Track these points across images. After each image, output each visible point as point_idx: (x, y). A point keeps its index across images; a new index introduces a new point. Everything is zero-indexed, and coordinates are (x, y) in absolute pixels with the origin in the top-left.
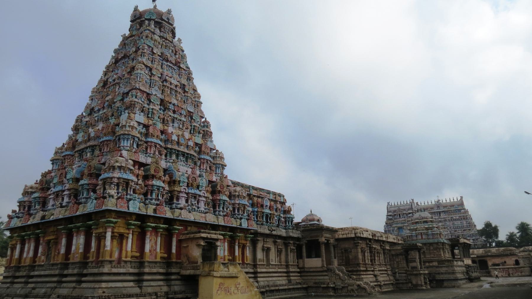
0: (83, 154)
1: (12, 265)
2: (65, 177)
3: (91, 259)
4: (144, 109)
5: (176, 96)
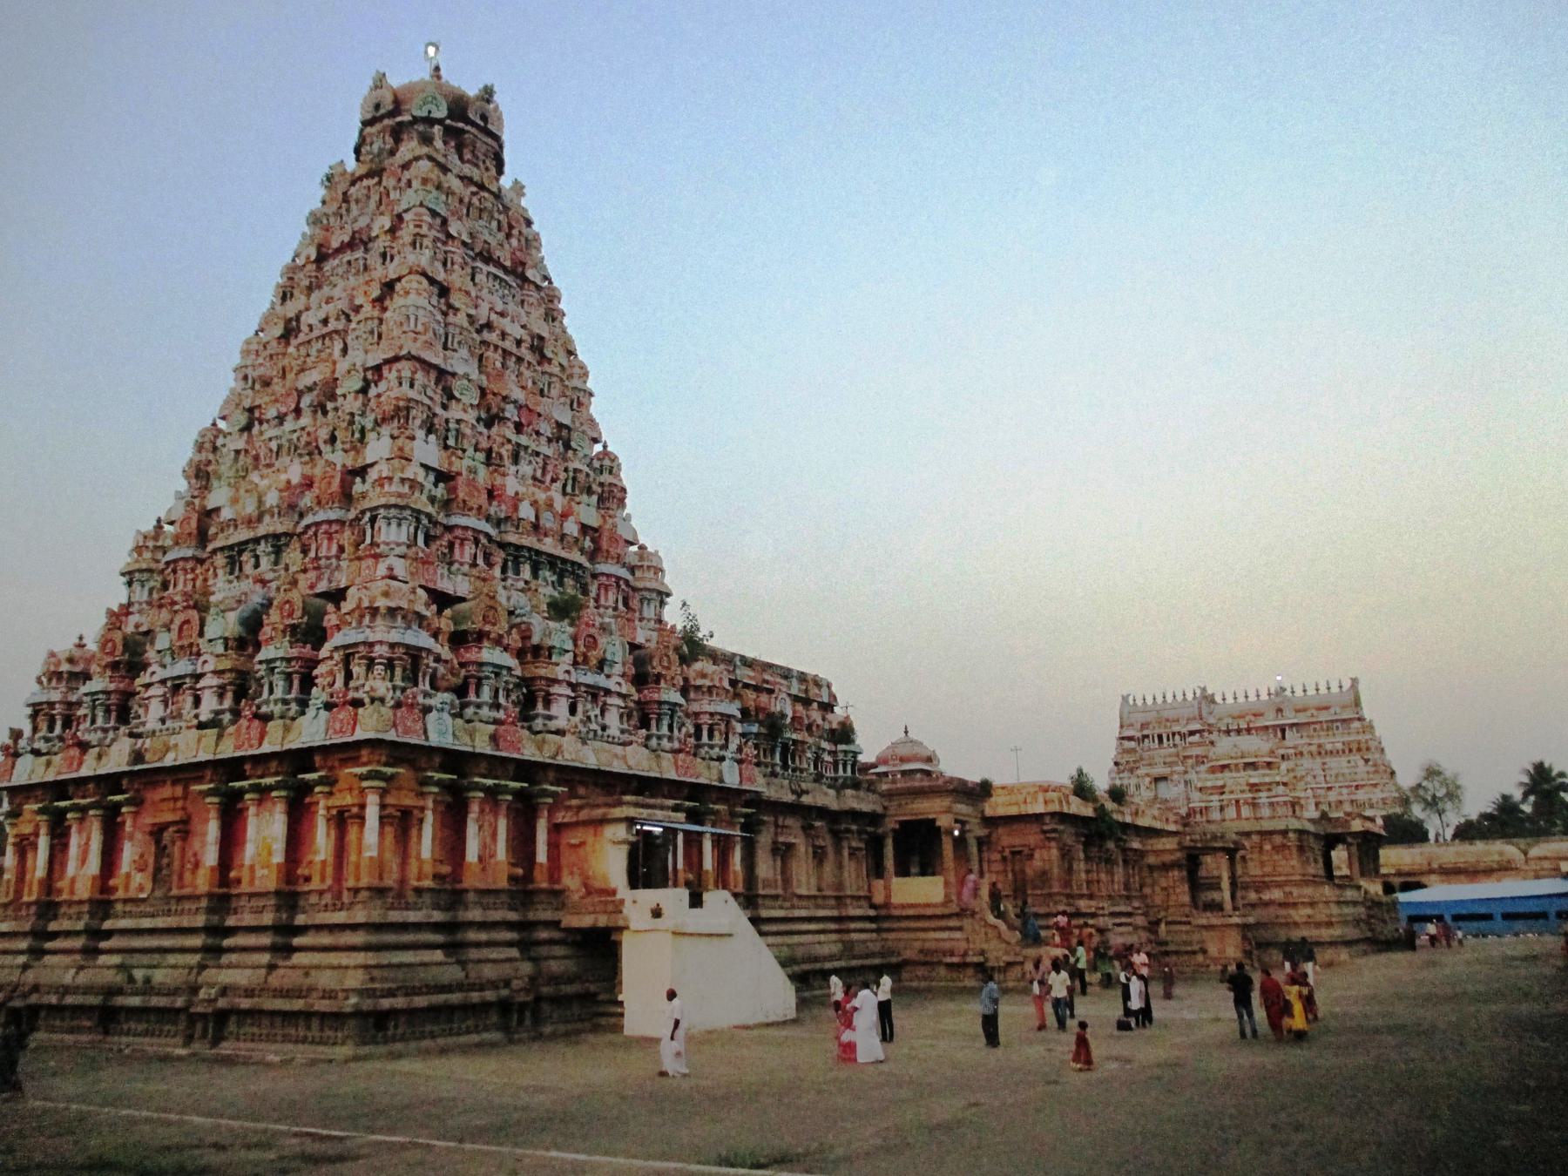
0: (244, 558)
1: (26, 899)
2: (201, 634)
3: (315, 884)
4: (436, 421)
5: (519, 375)
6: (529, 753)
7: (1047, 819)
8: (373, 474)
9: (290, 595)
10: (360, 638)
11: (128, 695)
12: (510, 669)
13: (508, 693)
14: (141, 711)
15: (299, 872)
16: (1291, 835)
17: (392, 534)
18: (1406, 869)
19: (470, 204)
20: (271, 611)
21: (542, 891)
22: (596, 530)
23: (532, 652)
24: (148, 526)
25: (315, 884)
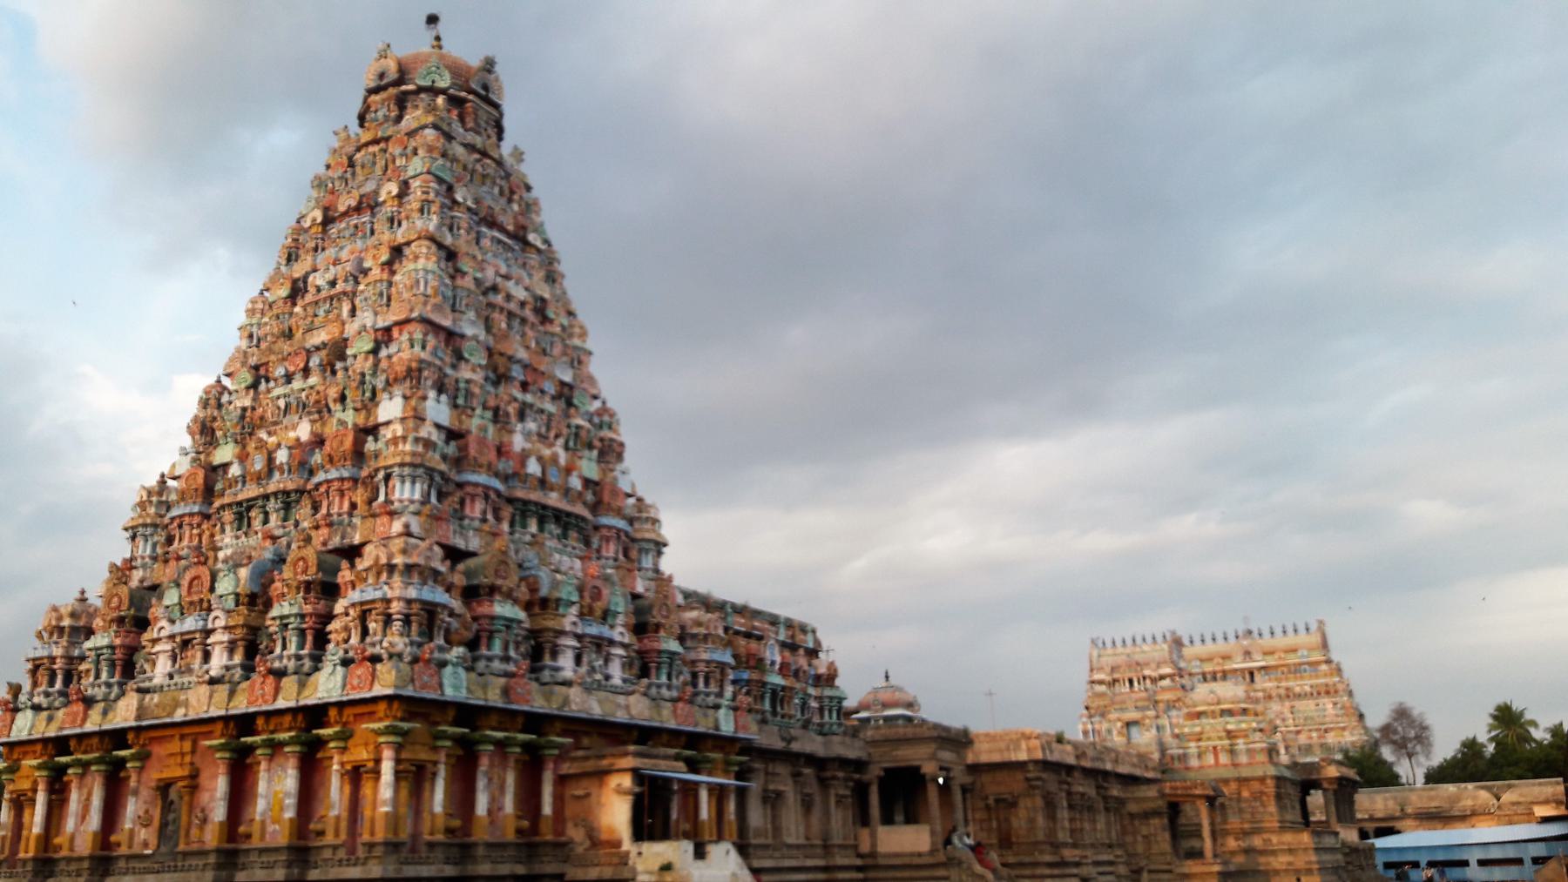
0: (253, 514)
1: (22, 855)
2: (212, 589)
3: (329, 839)
4: (446, 381)
6: (538, 704)
7: (1031, 767)
8: (386, 433)
9: (304, 552)
10: (378, 594)
11: (132, 650)
12: (520, 622)
13: (517, 644)
14: (147, 667)
15: (312, 826)
16: (1269, 781)
17: (406, 492)
18: (1379, 815)
19: (473, 171)
20: (285, 568)
21: (546, 843)
22: (596, 484)
23: (540, 605)
24: (152, 481)
25: (329, 839)
